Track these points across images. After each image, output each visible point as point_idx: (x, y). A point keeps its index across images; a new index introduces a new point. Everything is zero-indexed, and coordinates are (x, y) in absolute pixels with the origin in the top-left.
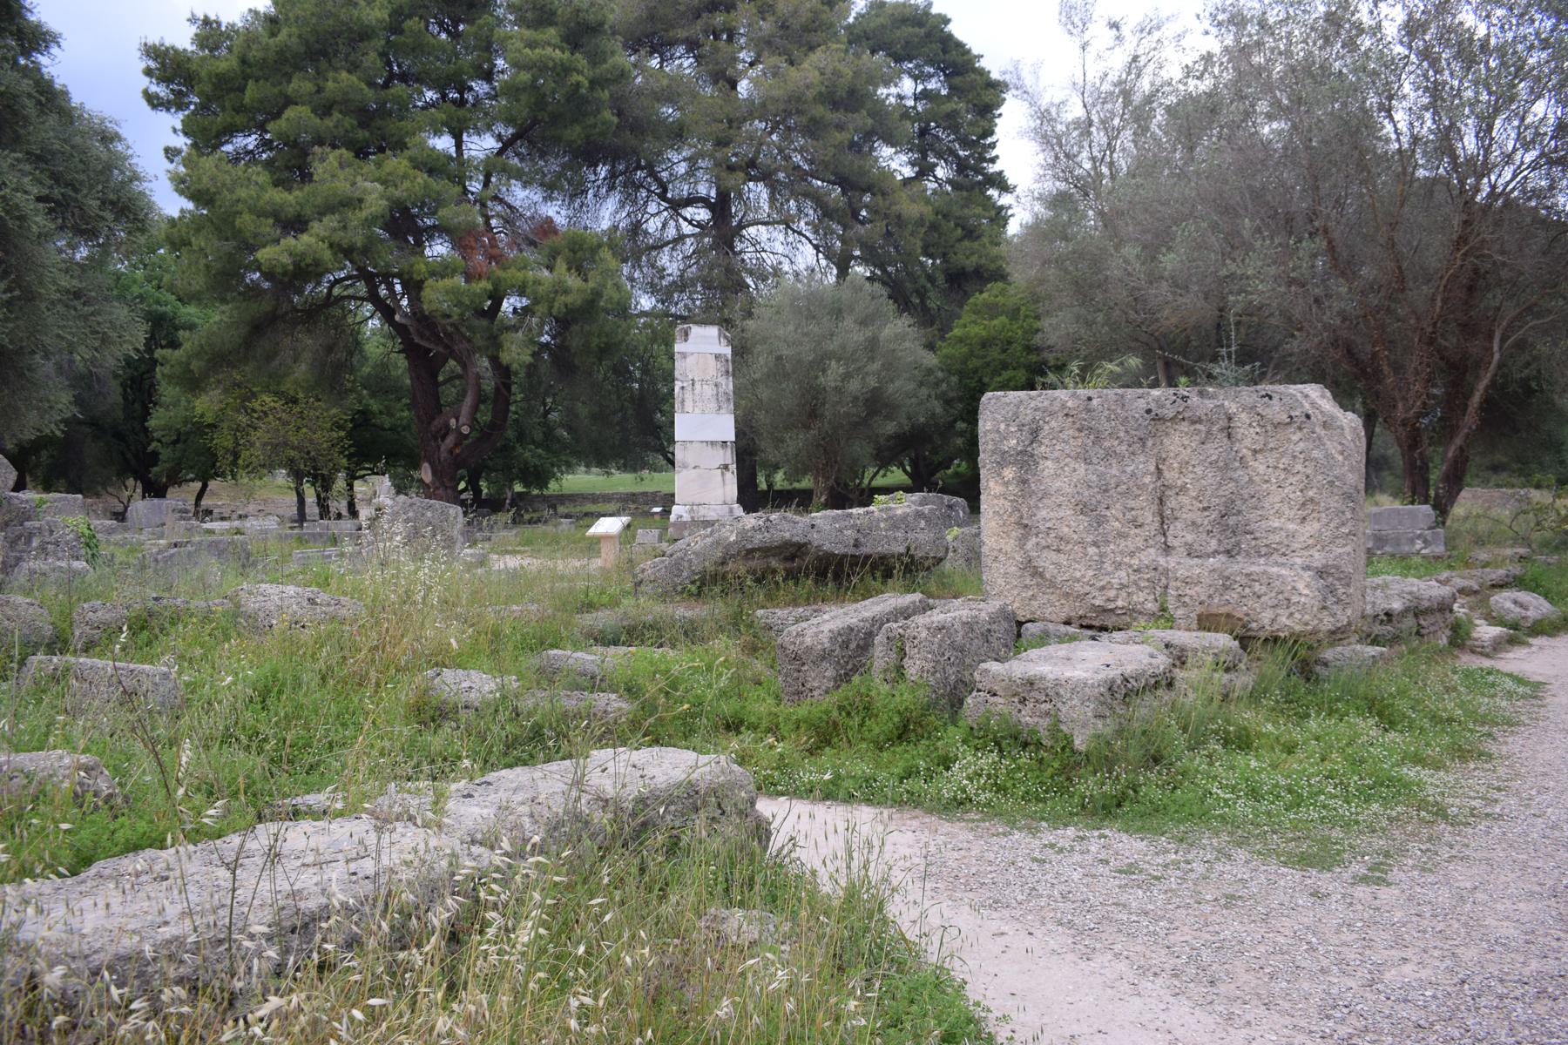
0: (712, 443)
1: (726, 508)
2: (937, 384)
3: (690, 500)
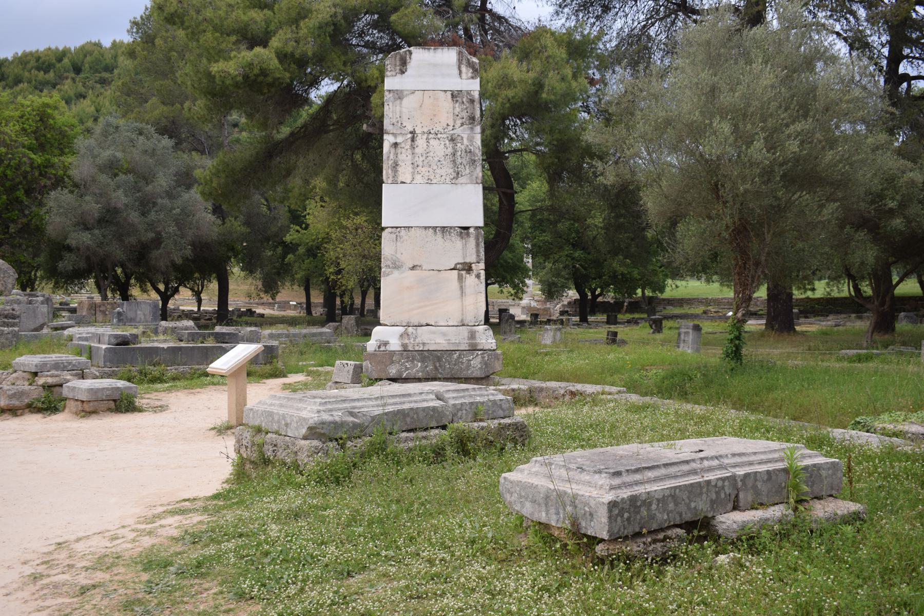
1: (464, 331)
3: (405, 318)
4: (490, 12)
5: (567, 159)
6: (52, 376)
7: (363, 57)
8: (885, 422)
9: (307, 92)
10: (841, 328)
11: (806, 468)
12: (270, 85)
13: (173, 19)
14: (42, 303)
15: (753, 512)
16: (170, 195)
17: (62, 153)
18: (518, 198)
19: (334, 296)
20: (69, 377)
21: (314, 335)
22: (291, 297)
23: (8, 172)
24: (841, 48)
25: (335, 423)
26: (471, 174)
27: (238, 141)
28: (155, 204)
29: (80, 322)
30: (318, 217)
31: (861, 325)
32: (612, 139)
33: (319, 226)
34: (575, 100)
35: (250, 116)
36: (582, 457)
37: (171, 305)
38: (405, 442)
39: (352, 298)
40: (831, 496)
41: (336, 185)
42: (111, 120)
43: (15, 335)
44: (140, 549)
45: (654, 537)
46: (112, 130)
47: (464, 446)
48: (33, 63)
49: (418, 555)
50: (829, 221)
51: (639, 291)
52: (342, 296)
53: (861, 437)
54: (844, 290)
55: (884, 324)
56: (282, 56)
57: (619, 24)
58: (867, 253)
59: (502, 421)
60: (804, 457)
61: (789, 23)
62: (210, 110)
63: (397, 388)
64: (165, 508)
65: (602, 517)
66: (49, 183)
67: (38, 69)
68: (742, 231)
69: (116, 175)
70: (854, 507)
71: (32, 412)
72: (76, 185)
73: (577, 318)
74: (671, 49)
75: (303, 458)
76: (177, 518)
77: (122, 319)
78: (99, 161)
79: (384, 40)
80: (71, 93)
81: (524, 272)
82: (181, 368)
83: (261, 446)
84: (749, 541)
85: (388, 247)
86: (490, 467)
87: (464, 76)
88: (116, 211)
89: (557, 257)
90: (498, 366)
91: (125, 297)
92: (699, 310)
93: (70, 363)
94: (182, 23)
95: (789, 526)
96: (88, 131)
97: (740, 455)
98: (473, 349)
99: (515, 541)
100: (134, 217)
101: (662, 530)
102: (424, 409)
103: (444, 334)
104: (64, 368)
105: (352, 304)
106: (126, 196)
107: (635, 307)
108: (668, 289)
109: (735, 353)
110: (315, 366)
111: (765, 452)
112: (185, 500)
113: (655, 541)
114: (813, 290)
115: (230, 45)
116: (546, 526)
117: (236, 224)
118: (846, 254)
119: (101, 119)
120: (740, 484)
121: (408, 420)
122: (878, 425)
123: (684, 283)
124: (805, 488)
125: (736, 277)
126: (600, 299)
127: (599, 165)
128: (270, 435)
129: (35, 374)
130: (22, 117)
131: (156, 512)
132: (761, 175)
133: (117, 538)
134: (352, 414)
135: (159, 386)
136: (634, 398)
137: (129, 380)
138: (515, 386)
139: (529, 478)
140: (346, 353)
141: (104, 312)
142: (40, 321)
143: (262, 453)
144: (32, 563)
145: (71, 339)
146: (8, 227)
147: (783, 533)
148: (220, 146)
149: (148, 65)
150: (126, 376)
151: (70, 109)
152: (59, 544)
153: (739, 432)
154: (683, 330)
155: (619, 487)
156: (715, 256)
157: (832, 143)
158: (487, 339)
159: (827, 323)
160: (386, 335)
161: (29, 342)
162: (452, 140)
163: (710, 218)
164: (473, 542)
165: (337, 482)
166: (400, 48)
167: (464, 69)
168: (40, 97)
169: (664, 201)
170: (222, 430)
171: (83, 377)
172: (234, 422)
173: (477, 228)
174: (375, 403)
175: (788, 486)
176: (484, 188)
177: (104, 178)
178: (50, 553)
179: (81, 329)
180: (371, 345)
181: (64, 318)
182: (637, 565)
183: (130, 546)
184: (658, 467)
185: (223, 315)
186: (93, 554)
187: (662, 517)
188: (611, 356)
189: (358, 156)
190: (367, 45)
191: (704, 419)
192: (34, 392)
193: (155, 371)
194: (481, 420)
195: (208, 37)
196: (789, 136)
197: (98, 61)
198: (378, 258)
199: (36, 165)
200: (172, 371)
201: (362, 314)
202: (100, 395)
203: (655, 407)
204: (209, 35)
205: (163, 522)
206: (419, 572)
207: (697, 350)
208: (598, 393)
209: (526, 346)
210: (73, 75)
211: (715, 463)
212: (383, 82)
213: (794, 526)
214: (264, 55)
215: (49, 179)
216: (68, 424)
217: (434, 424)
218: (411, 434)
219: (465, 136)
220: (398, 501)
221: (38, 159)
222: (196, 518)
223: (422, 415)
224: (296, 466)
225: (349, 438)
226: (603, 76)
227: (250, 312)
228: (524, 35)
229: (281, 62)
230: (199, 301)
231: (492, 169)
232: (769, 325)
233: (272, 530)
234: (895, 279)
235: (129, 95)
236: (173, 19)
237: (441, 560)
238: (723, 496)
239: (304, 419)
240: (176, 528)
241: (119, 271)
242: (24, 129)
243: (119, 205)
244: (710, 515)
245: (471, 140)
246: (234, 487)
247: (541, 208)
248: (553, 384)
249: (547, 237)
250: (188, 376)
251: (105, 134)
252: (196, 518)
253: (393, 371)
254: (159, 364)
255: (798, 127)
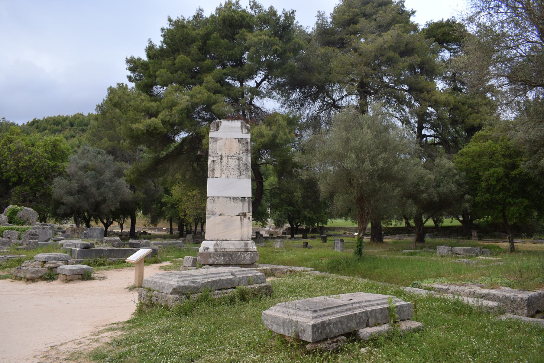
0: (234, 198)
1: (243, 243)
2: (454, 176)
3: (216, 237)
4: (254, 105)
5: (286, 168)
6: (52, 263)
7: (198, 123)
8: (425, 283)
9: (174, 137)
10: (402, 240)
11: (397, 307)
12: (158, 134)
13: (116, 105)
14: (50, 229)
15: (375, 328)
16: (111, 180)
17: (63, 161)
18: (265, 184)
19: (183, 226)
20: (60, 264)
21: (174, 243)
22: (163, 226)
23: (37, 169)
24: (399, 124)
25: (185, 287)
26: (246, 174)
27: (142, 157)
28: (104, 184)
29: (67, 238)
30: (177, 191)
31: (411, 239)
32: (305, 160)
33: (177, 194)
34: (289, 142)
35: (149, 147)
36: (299, 303)
37: (109, 229)
38: (217, 295)
39: (191, 227)
40: (408, 319)
41: (185, 177)
42: (86, 147)
43: (36, 244)
44: (92, 349)
45: (333, 340)
46: (86, 151)
47: (244, 297)
48: (52, 122)
49: (224, 350)
50: (397, 195)
51: (316, 224)
52: (186, 226)
53: (418, 291)
54: (403, 224)
55: (420, 239)
56: (164, 122)
57: (307, 112)
58: (414, 209)
59: (261, 285)
60: (396, 302)
61: (376, 114)
62: (131, 144)
63: (213, 270)
64: (104, 328)
65: (309, 332)
66: (56, 174)
67: (54, 124)
68: (361, 200)
69: (87, 171)
70: (418, 324)
71: (42, 280)
72: (68, 176)
73: (290, 236)
74: (329, 123)
75: (170, 303)
76: (110, 333)
77: (87, 236)
78: (79, 165)
79: (208, 116)
80: (69, 135)
81: (267, 216)
82: (113, 259)
83: (151, 297)
84: (374, 341)
85: (209, 205)
86: (256, 306)
87: (244, 132)
88: (86, 187)
89: (281, 209)
90: (257, 259)
91: (88, 226)
92: (342, 232)
93: (61, 257)
94: (120, 107)
95: (391, 334)
96: (75, 151)
97: (369, 301)
98: (247, 251)
99: (269, 343)
100: (94, 190)
101: (336, 337)
102: (226, 280)
103: (234, 244)
104: (59, 260)
105: (191, 229)
106: (91, 181)
107: (314, 231)
108: (328, 223)
109: (359, 252)
110: (174, 258)
111: (379, 300)
112: (114, 324)
113: (333, 342)
114: (391, 224)
115: (141, 117)
116: (283, 336)
117: (140, 193)
118: (404, 209)
119: (81, 146)
120: (369, 315)
121: (219, 285)
122: (423, 285)
123: (335, 221)
124: (397, 316)
125: (359, 219)
126: (299, 227)
127: (300, 170)
128: (155, 292)
129: (45, 262)
130: (45, 145)
131: (100, 330)
132: (369, 176)
133: (81, 344)
134: (193, 282)
135: (102, 267)
136: (318, 273)
137: (89, 265)
138: (265, 268)
139: (277, 313)
140: (188, 252)
141: (78, 233)
142: (49, 237)
143: (151, 301)
144: (38, 357)
145: (62, 245)
146: (35, 194)
147: (390, 337)
148: (134, 159)
149: (104, 124)
150: (87, 263)
151: (68, 142)
152: (52, 347)
153: (365, 289)
154: (336, 242)
155: (316, 317)
156: (349, 210)
157: (396, 163)
158: (253, 247)
159: (396, 238)
160: (207, 245)
161: (42, 247)
162: (238, 159)
163: (348, 194)
164: (249, 344)
165: (186, 314)
166: (215, 119)
167: (244, 129)
168: (54, 137)
169: (328, 186)
170: (132, 289)
171: (67, 263)
172: (137, 285)
173: (249, 197)
174: (204, 277)
175: (389, 315)
176: (252, 180)
177: (81, 173)
178: (47, 351)
179: (67, 241)
180: (201, 249)
181: (60, 235)
182: (325, 354)
183: (87, 347)
184: (333, 307)
185: (133, 234)
186: (69, 352)
187: (336, 331)
188: (306, 253)
189: (195, 165)
190: (201, 118)
191: (349, 283)
192: (44, 271)
193: (101, 260)
194: (251, 285)
195: (131, 113)
196: (379, 159)
197: (81, 122)
198: (204, 209)
199: (50, 166)
200: (109, 260)
201: (195, 234)
202: (75, 272)
203: (327, 277)
204: (131, 112)
205: (103, 335)
206: (225, 359)
207: (342, 250)
208: (302, 271)
209: (269, 249)
210: (70, 127)
211: (358, 305)
212: (208, 134)
213: (394, 334)
214: (156, 121)
215: (56, 172)
216: (59, 286)
217: (230, 286)
218: (220, 291)
219: (244, 158)
220: (214, 324)
221: (51, 164)
222: (119, 333)
223: (225, 282)
224: (167, 307)
225: (191, 294)
226: (301, 133)
227: (145, 233)
228: (268, 115)
229: (163, 124)
230: (122, 228)
231: (254, 173)
232: (373, 239)
233: (155, 339)
234: (424, 220)
235: (94, 137)
236: (116, 105)
237: (235, 353)
238: (362, 320)
239: (171, 285)
240: (109, 338)
241: (86, 214)
242: (46, 151)
243: (87, 185)
244: (356, 330)
245: (246, 159)
246: (137, 317)
247: (275, 188)
248: (282, 267)
249: (277, 201)
250: (116, 263)
251: (83, 153)
252: (119, 333)
253: (210, 261)
254: (103, 257)
255: (383, 155)
